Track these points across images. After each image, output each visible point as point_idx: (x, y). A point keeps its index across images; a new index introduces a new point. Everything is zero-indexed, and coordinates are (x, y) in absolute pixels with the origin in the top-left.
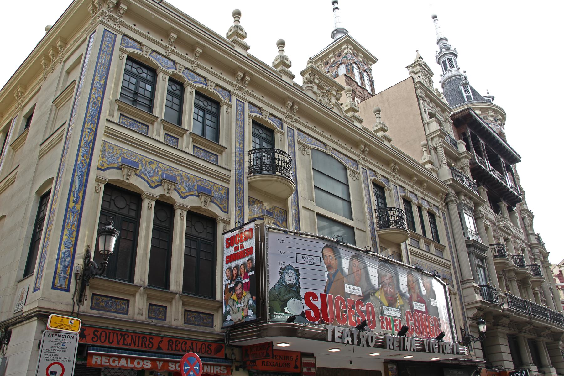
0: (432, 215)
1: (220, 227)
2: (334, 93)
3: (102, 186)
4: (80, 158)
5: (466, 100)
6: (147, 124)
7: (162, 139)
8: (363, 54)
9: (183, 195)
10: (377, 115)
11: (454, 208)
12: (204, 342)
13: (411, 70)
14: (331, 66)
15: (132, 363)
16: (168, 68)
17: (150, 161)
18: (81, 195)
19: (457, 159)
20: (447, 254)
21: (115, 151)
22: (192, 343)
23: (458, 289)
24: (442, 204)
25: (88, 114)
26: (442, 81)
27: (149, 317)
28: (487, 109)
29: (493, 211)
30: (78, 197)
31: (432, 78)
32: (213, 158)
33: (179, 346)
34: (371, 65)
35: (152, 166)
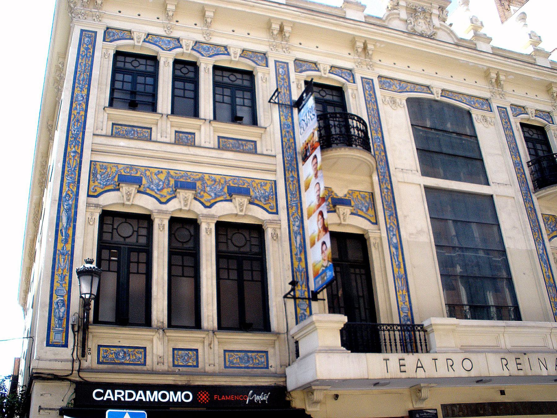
4: (65, 188)
6: (149, 126)
9: (208, 204)
18: (70, 232)
21: (109, 170)
25: (70, 135)
30: (67, 235)
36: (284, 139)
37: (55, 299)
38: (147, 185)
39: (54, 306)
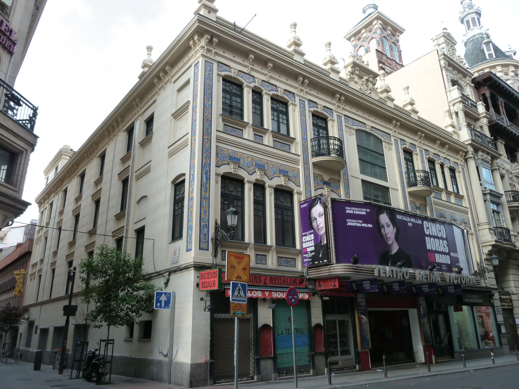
0: (452, 170)
1: (296, 198)
2: (371, 79)
3: (220, 178)
4: (204, 160)
5: (488, 58)
7: (252, 138)
8: (392, 27)
9: (270, 178)
10: (406, 91)
11: (472, 164)
12: (291, 278)
13: (436, 42)
14: (363, 41)
15: (251, 293)
16: (250, 83)
17: (246, 156)
18: (208, 186)
19: (477, 119)
20: (465, 203)
22: (285, 279)
23: (475, 230)
24: (462, 161)
26: (465, 40)
27: (256, 263)
28: (507, 65)
29: (509, 161)
30: (206, 188)
31: (455, 46)
32: (287, 147)
33: (277, 281)
34: (398, 36)
35: (248, 159)
36: (206, 114)
37: (202, 224)
38: (242, 163)
39: (202, 227)
